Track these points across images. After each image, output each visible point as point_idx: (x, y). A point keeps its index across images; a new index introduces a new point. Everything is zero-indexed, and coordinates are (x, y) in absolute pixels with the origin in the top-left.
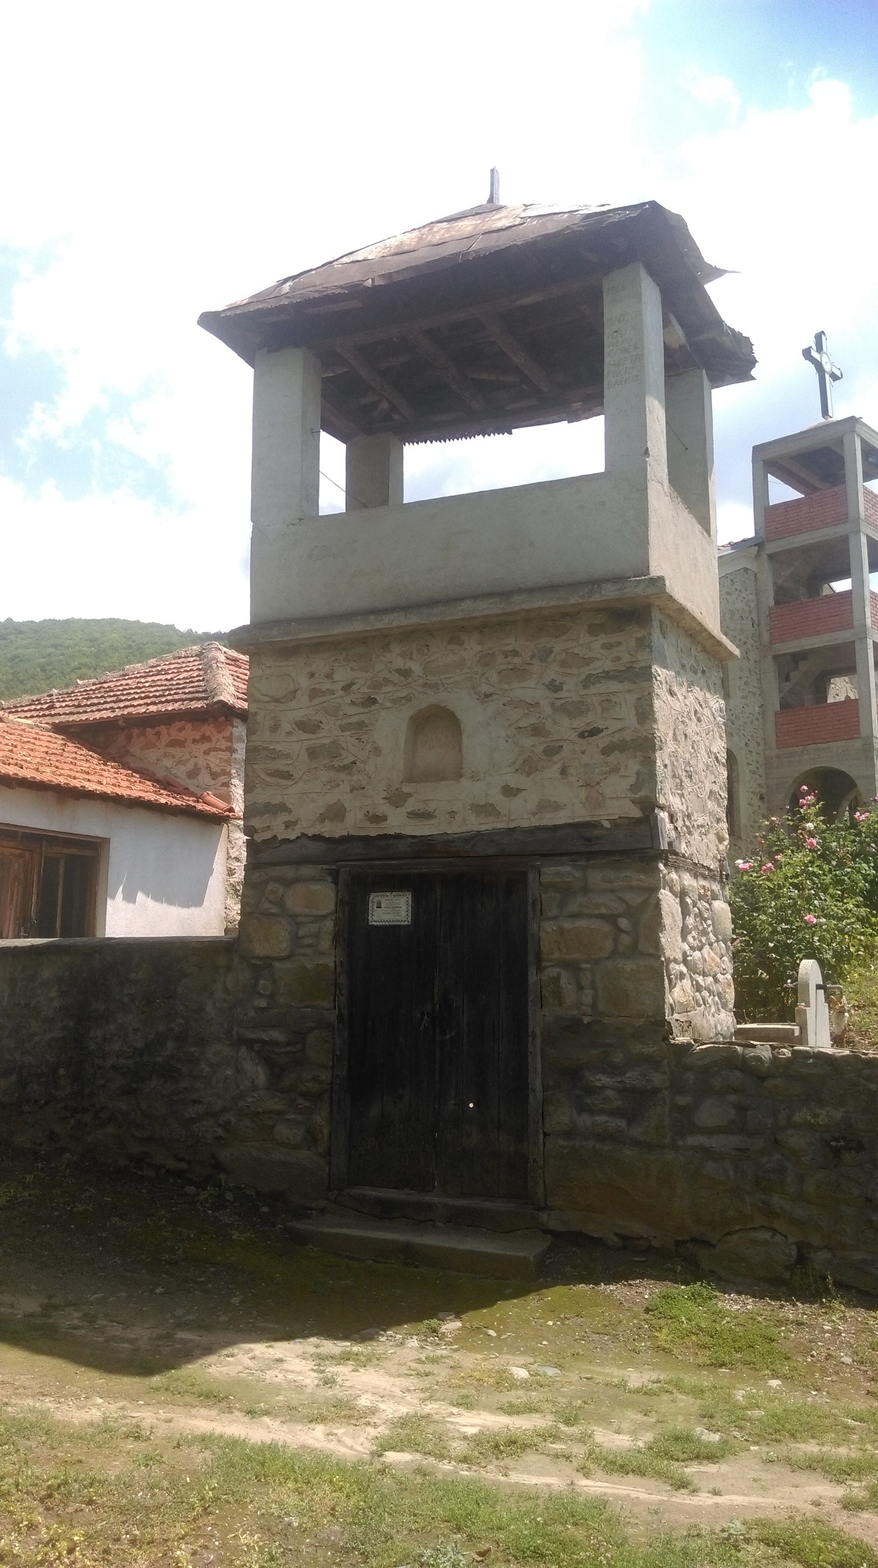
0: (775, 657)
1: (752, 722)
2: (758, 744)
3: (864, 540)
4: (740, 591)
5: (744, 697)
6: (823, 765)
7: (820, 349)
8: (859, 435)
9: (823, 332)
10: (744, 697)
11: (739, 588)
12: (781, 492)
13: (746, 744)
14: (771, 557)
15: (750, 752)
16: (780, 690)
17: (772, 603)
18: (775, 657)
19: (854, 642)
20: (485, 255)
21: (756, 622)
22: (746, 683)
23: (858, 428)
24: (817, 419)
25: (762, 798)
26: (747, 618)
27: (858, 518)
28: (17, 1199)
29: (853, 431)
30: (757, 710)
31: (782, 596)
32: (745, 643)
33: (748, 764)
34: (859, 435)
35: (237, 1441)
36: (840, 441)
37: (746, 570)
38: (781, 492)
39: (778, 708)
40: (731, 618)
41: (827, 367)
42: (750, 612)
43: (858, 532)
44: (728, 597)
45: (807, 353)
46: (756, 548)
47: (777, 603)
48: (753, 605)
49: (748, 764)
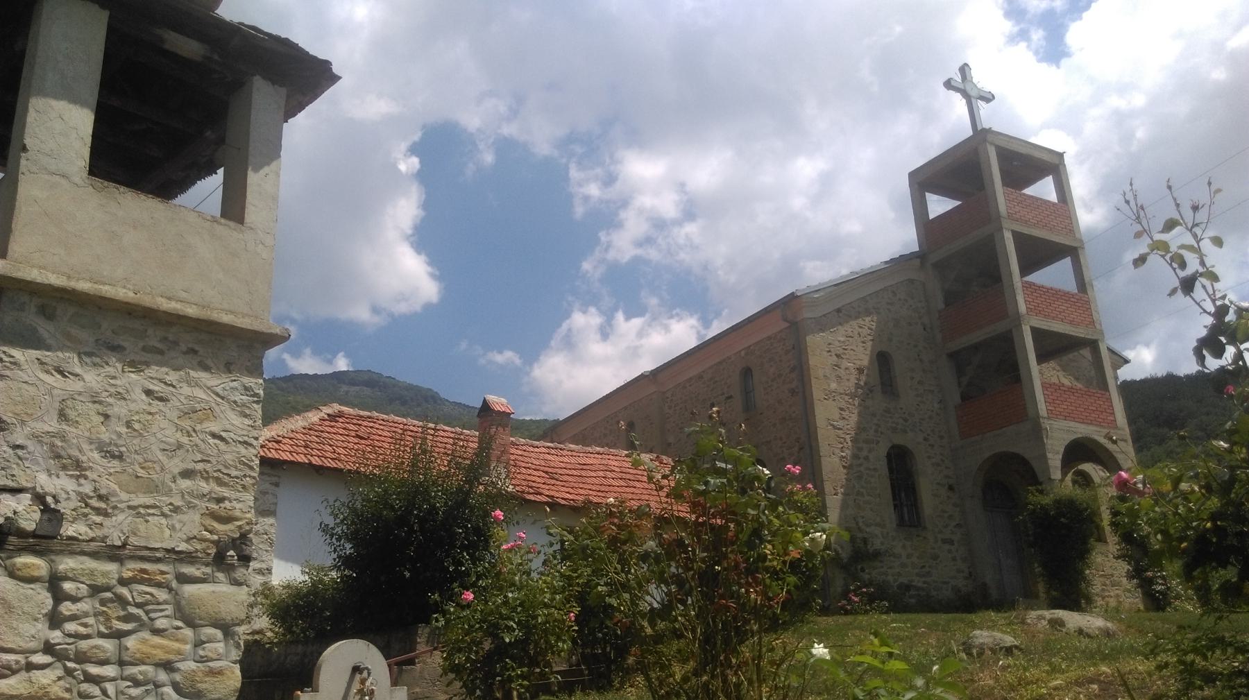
0: (953, 356)
2: (941, 437)
3: (1008, 236)
6: (1004, 449)
8: (991, 144)
12: (938, 205)
13: (925, 439)
14: (936, 266)
15: (932, 446)
16: (959, 384)
17: (941, 306)
18: (953, 356)
19: (1011, 331)
20: (429, 264)
23: (990, 137)
25: (951, 488)
27: (999, 216)
30: (936, 405)
31: (951, 298)
32: (916, 346)
33: (929, 457)
35: (288, 606)
36: (976, 152)
37: (911, 281)
38: (938, 205)
39: (957, 399)
41: (973, 93)
43: (1000, 229)
46: (919, 260)
47: (947, 304)
49: (929, 457)
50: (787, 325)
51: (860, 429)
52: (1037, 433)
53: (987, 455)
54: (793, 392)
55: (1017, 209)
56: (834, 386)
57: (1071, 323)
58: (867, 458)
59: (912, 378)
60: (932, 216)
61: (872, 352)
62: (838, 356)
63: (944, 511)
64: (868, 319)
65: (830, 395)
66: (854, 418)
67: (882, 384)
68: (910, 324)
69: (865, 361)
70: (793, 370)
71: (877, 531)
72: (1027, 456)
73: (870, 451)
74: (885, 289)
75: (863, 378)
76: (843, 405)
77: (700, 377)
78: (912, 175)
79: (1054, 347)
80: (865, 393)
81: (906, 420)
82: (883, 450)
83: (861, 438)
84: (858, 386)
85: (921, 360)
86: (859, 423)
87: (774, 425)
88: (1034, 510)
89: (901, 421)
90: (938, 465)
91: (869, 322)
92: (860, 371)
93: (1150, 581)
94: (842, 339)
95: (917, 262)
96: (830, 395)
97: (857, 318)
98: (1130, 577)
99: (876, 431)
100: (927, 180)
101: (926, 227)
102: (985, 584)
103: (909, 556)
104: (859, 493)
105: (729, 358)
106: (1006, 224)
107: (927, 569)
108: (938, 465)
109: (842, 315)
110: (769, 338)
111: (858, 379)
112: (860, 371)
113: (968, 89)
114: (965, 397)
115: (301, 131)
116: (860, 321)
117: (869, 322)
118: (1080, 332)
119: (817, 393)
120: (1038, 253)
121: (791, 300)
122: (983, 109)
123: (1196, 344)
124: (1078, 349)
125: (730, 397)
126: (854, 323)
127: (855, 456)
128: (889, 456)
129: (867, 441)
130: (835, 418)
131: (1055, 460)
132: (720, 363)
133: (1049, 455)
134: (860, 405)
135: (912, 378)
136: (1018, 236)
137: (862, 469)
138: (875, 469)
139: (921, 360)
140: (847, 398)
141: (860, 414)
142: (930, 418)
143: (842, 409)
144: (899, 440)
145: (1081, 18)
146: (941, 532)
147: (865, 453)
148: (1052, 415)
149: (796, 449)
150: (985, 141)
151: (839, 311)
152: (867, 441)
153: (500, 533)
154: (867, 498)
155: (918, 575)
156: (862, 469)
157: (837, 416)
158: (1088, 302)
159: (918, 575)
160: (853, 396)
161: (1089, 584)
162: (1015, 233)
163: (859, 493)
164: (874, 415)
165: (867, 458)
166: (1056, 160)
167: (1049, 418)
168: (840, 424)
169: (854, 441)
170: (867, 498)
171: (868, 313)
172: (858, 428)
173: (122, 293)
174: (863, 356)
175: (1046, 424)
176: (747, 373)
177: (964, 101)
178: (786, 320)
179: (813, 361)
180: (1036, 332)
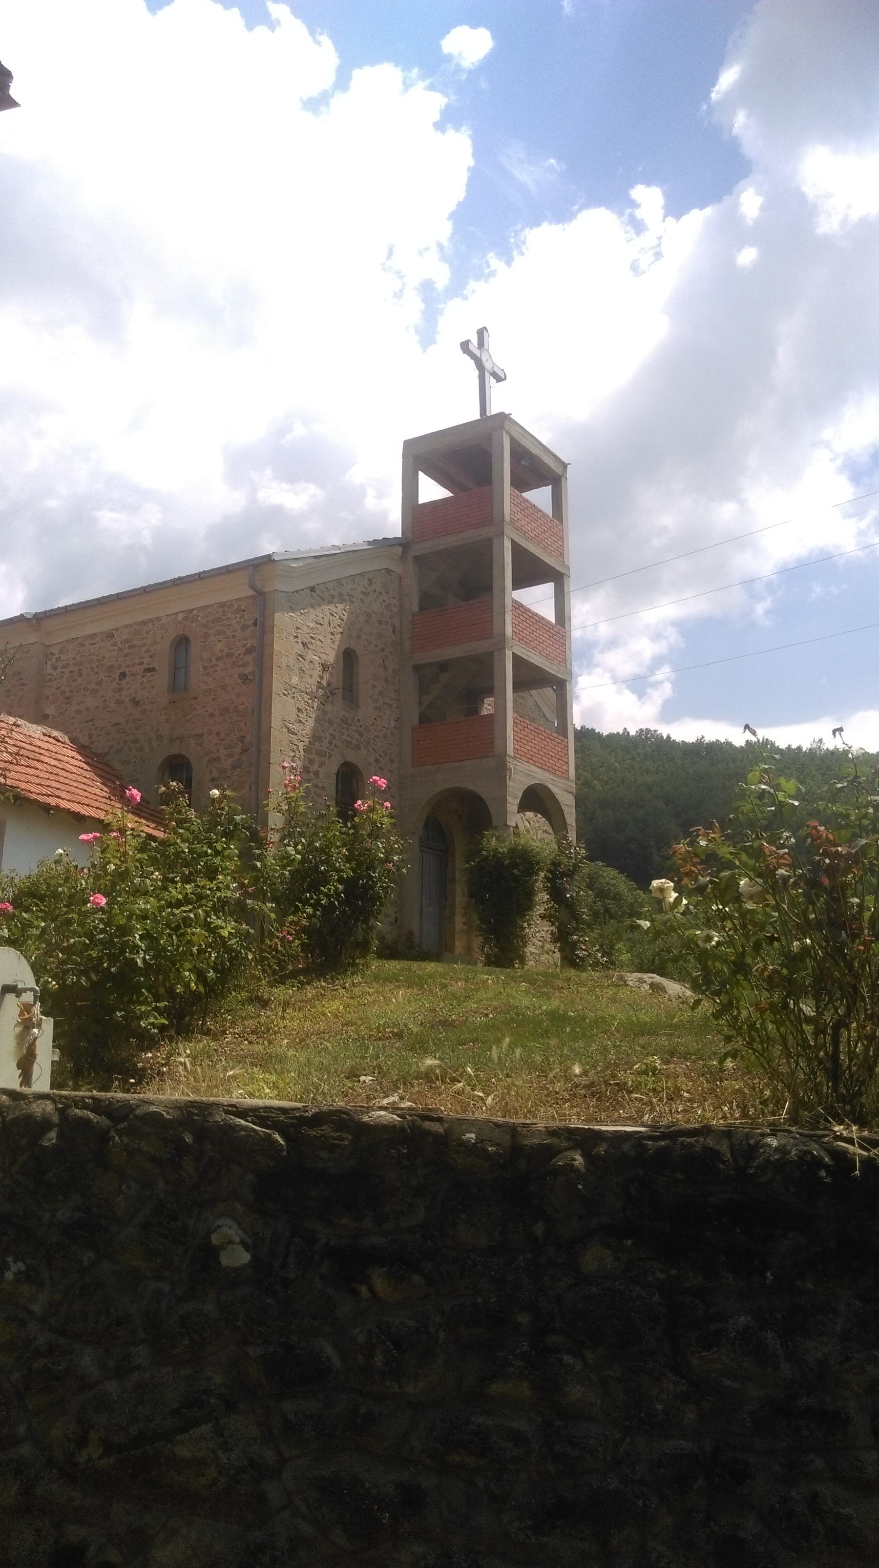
0: (417, 668)
1: (385, 736)
2: (392, 761)
3: (507, 544)
4: (380, 593)
5: (376, 708)
6: (462, 785)
7: (481, 344)
9: (485, 328)
10: (376, 708)
11: (378, 589)
12: (431, 491)
13: (377, 760)
14: (416, 559)
17: (415, 608)
18: (417, 668)
21: (398, 628)
22: (381, 693)
23: (507, 425)
24: (473, 414)
26: (387, 623)
28: (783, 961)
29: (502, 428)
30: (393, 723)
31: (427, 601)
32: (383, 650)
34: (508, 433)
36: (489, 438)
37: (388, 571)
38: (431, 491)
39: (416, 722)
40: (367, 621)
41: (488, 366)
42: (391, 617)
44: (363, 597)
45: (465, 346)
46: (400, 549)
47: (422, 609)
48: (395, 610)
50: (252, 593)
51: (316, 737)
52: (501, 772)
54: (245, 679)
55: (520, 516)
56: (295, 680)
57: (547, 656)
59: (374, 687)
60: (420, 502)
61: (339, 646)
62: (304, 644)
64: (340, 606)
65: (290, 690)
66: (311, 723)
67: (344, 688)
68: (380, 622)
69: (331, 658)
70: (249, 651)
72: (483, 796)
73: (321, 766)
75: (327, 676)
76: (302, 705)
77: (110, 635)
79: (530, 678)
80: (328, 694)
81: (361, 735)
82: (334, 768)
83: (315, 747)
84: (319, 686)
85: (385, 667)
86: (315, 730)
87: (212, 715)
88: (487, 858)
89: (356, 735)
91: (341, 610)
92: (324, 667)
93: (574, 946)
94: (312, 625)
95: (399, 550)
96: (290, 690)
97: (330, 602)
98: (555, 940)
99: (330, 743)
100: (422, 456)
101: (413, 510)
102: (411, 933)
105: (159, 619)
106: (508, 531)
109: (316, 595)
110: (222, 605)
111: (321, 677)
112: (324, 667)
113: (484, 359)
114: (424, 720)
115: (503, 263)
116: (332, 607)
117: (341, 610)
118: (551, 668)
119: (277, 686)
120: (531, 571)
121: (262, 565)
122: (495, 390)
124: (546, 683)
125: (153, 670)
126: (326, 608)
127: (306, 769)
129: (320, 754)
130: (292, 718)
131: (513, 803)
132: (144, 623)
133: (509, 799)
134: (318, 709)
135: (374, 687)
136: (516, 548)
138: (323, 788)
139: (385, 667)
140: (306, 697)
141: (317, 720)
143: (299, 710)
144: (351, 757)
147: (315, 767)
149: (238, 750)
150: (501, 427)
151: (312, 589)
152: (320, 754)
157: (293, 718)
158: (564, 637)
160: (313, 697)
161: (525, 942)
162: (514, 544)
164: (331, 722)
165: (316, 773)
166: (559, 470)
167: (514, 758)
168: (295, 727)
169: (307, 750)
171: (342, 601)
172: (314, 735)
174: (328, 651)
175: (511, 764)
176: (182, 642)
177: (477, 373)
178: (252, 587)
179: (279, 645)
180: (515, 657)
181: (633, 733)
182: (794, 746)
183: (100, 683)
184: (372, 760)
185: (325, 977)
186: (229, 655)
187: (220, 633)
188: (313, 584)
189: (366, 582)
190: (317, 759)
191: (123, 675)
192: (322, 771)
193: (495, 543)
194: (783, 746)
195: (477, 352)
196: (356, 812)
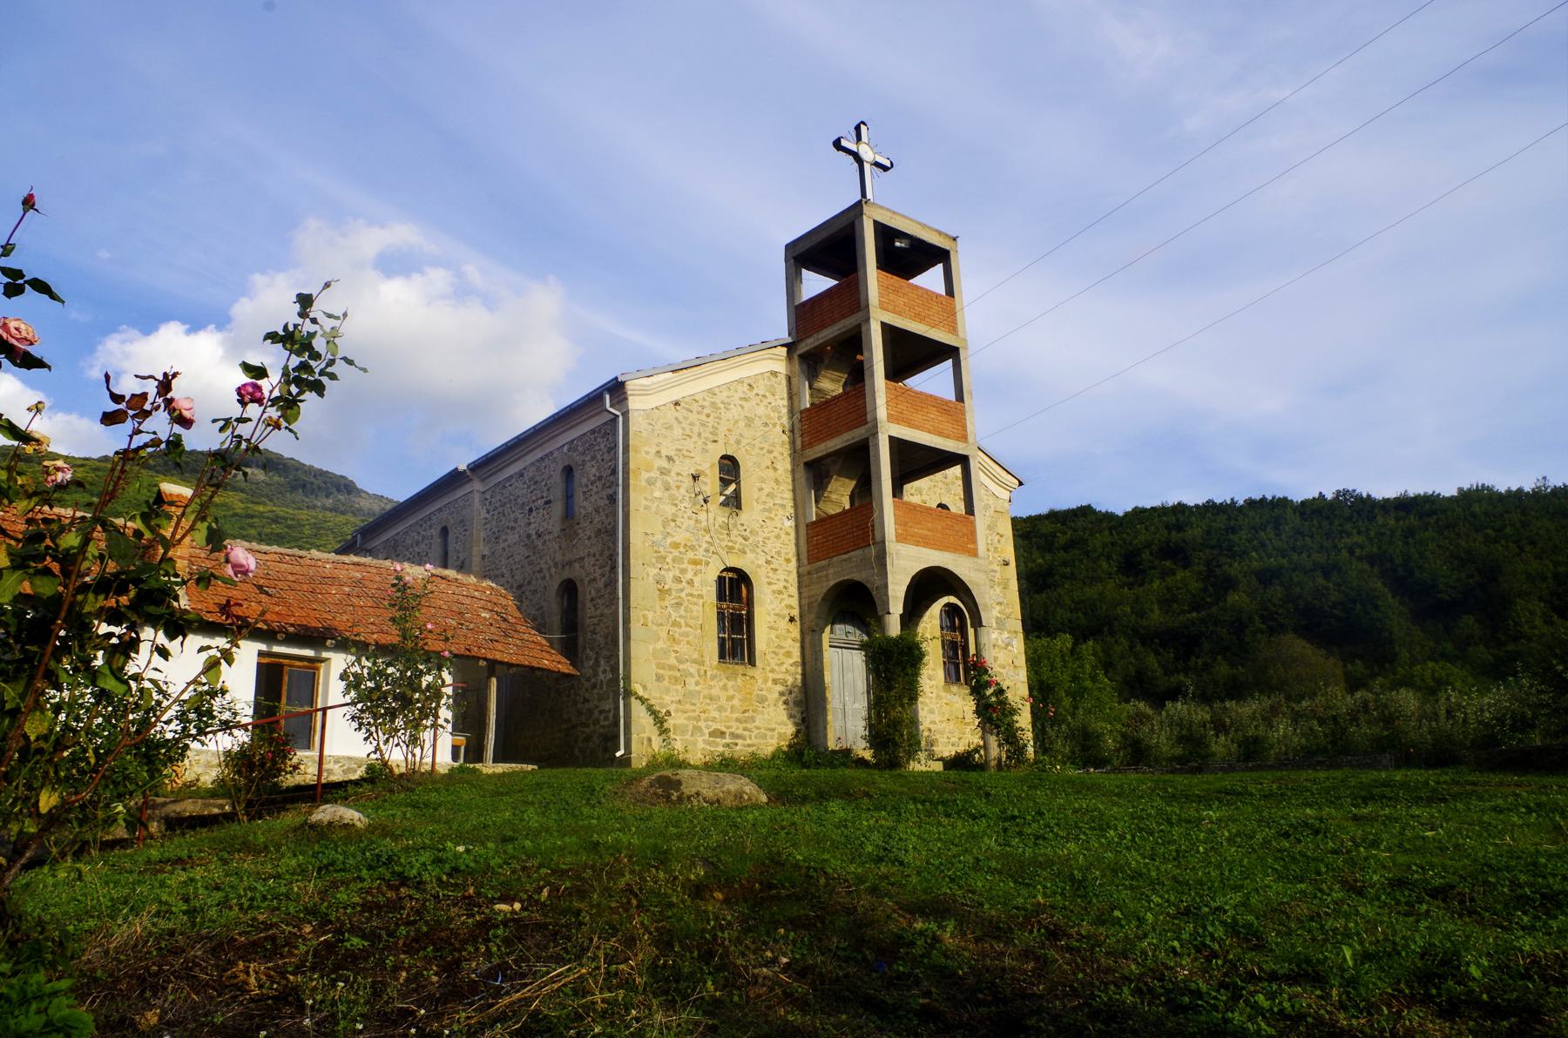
10: (765, 510)
12: (815, 284)
38: (815, 284)
40: (748, 425)
46: (785, 350)
53: (832, 583)
58: (690, 583)
63: (780, 647)
71: (693, 669)
74: (740, 381)
78: (787, 246)
82: (713, 573)
90: (780, 592)
99: (707, 551)
100: (804, 254)
103: (730, 698)
104: (675, 624)
107: (750, 714)
108: (780, 592)
123: (1129, 509)
128: (721, 580)
137: (683, 595)
138: (700, 596)
142: (778, 537)
145: (1460, 490)
146: (772, 671)
147: (689, 576)
148: (901, 538)
151: (677, 404)
153: (947, 750)
154: (684, 629)
155: (738, 720)
156: (683, 595)
159: (738, 720)
163: (675, 624)
165: (690, 583)
170: (684, 629)
173: (632, 540)
177: (856, 165)
181: (1329, 496)
182: (1514, 488)
183: (516, 521)
184: (762, 561)
185: (1504, 681)
186: (600, 478)
187: (593, 458)
188: (675, 398)
189: (746, 387)
190: (690, 567)
191: (531, 510)
192: (697, 580)
193: (864, 329)
194: (1503, 490)
195: (853, 147)
196: (59, 661)
